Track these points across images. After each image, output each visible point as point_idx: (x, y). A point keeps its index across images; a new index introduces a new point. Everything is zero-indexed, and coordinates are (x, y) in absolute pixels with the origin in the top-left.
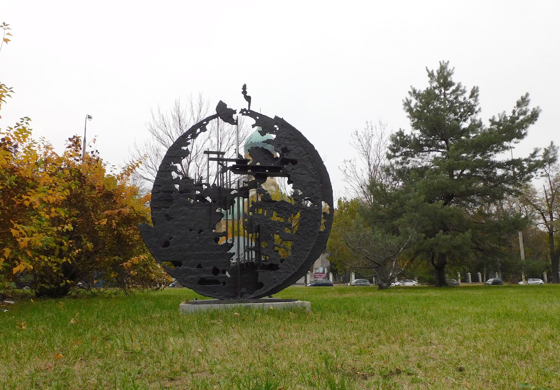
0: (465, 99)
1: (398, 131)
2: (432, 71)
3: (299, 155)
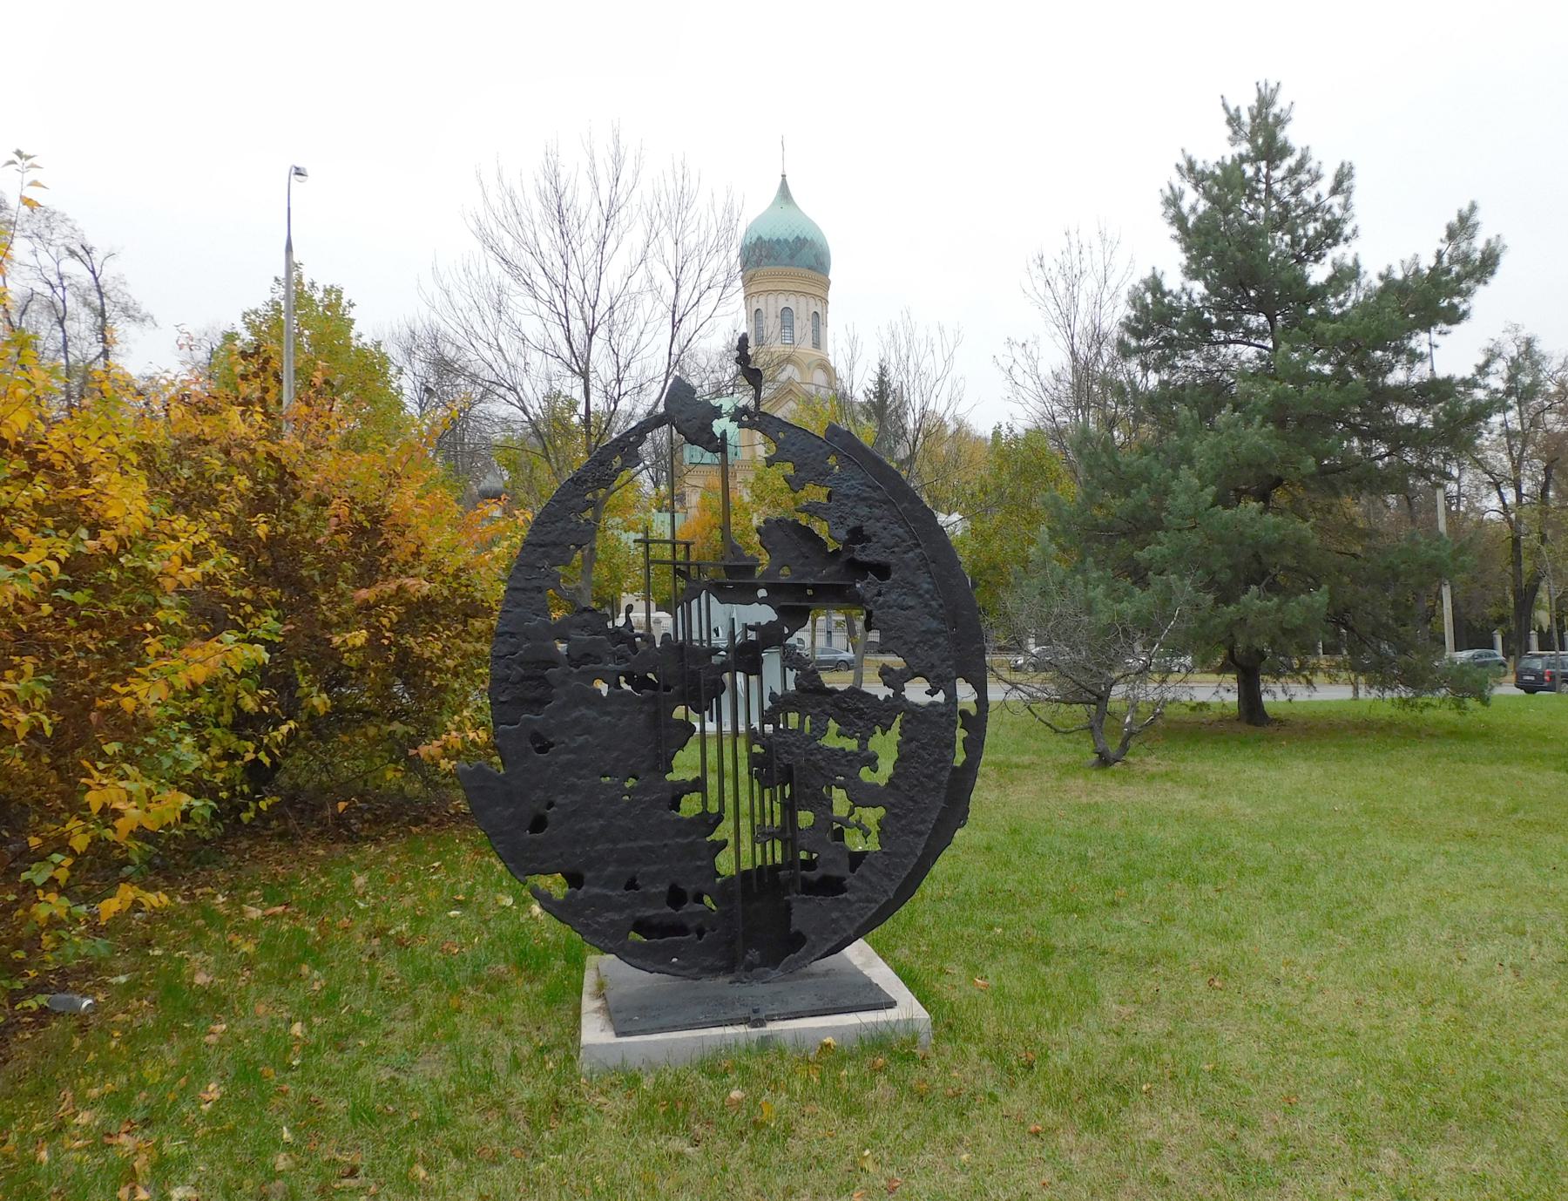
0: (1318, 197)
1: (1147, 274)
2: (1237, 110)
3: (896, 549)
